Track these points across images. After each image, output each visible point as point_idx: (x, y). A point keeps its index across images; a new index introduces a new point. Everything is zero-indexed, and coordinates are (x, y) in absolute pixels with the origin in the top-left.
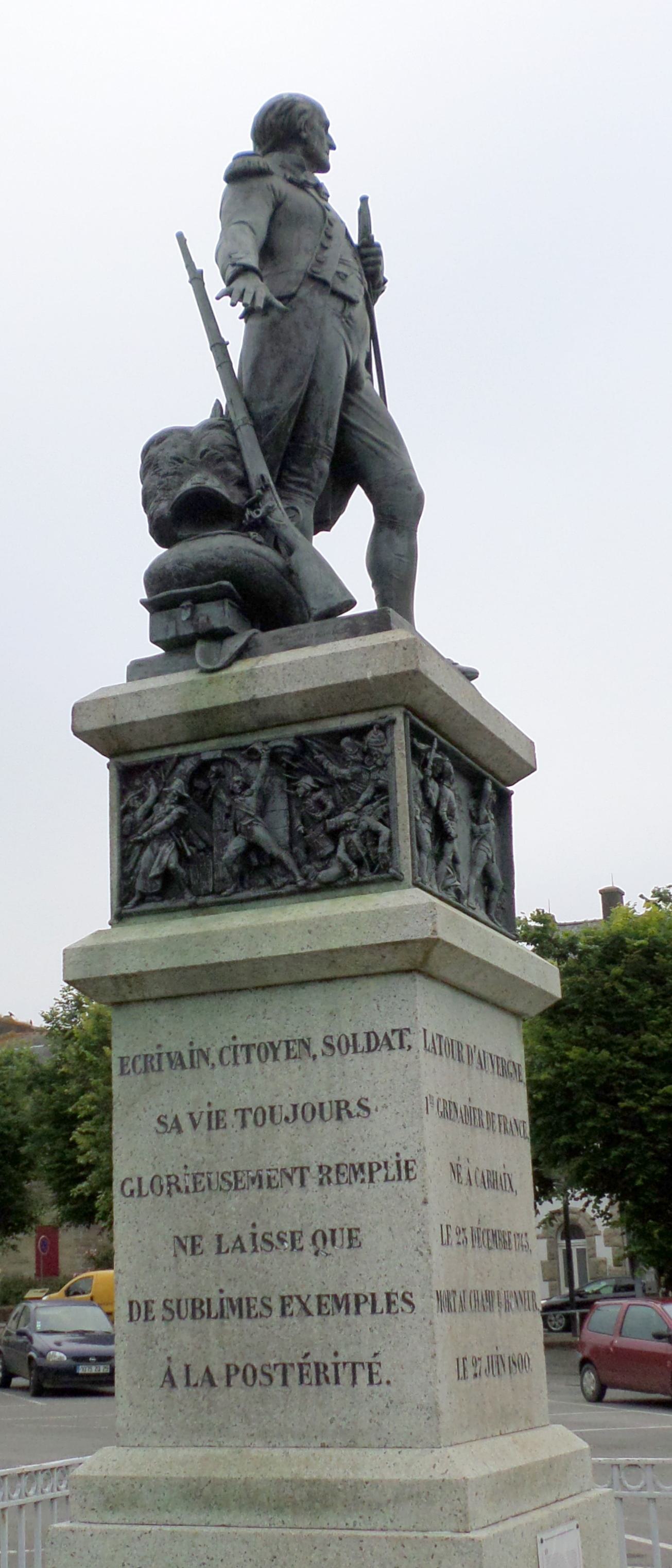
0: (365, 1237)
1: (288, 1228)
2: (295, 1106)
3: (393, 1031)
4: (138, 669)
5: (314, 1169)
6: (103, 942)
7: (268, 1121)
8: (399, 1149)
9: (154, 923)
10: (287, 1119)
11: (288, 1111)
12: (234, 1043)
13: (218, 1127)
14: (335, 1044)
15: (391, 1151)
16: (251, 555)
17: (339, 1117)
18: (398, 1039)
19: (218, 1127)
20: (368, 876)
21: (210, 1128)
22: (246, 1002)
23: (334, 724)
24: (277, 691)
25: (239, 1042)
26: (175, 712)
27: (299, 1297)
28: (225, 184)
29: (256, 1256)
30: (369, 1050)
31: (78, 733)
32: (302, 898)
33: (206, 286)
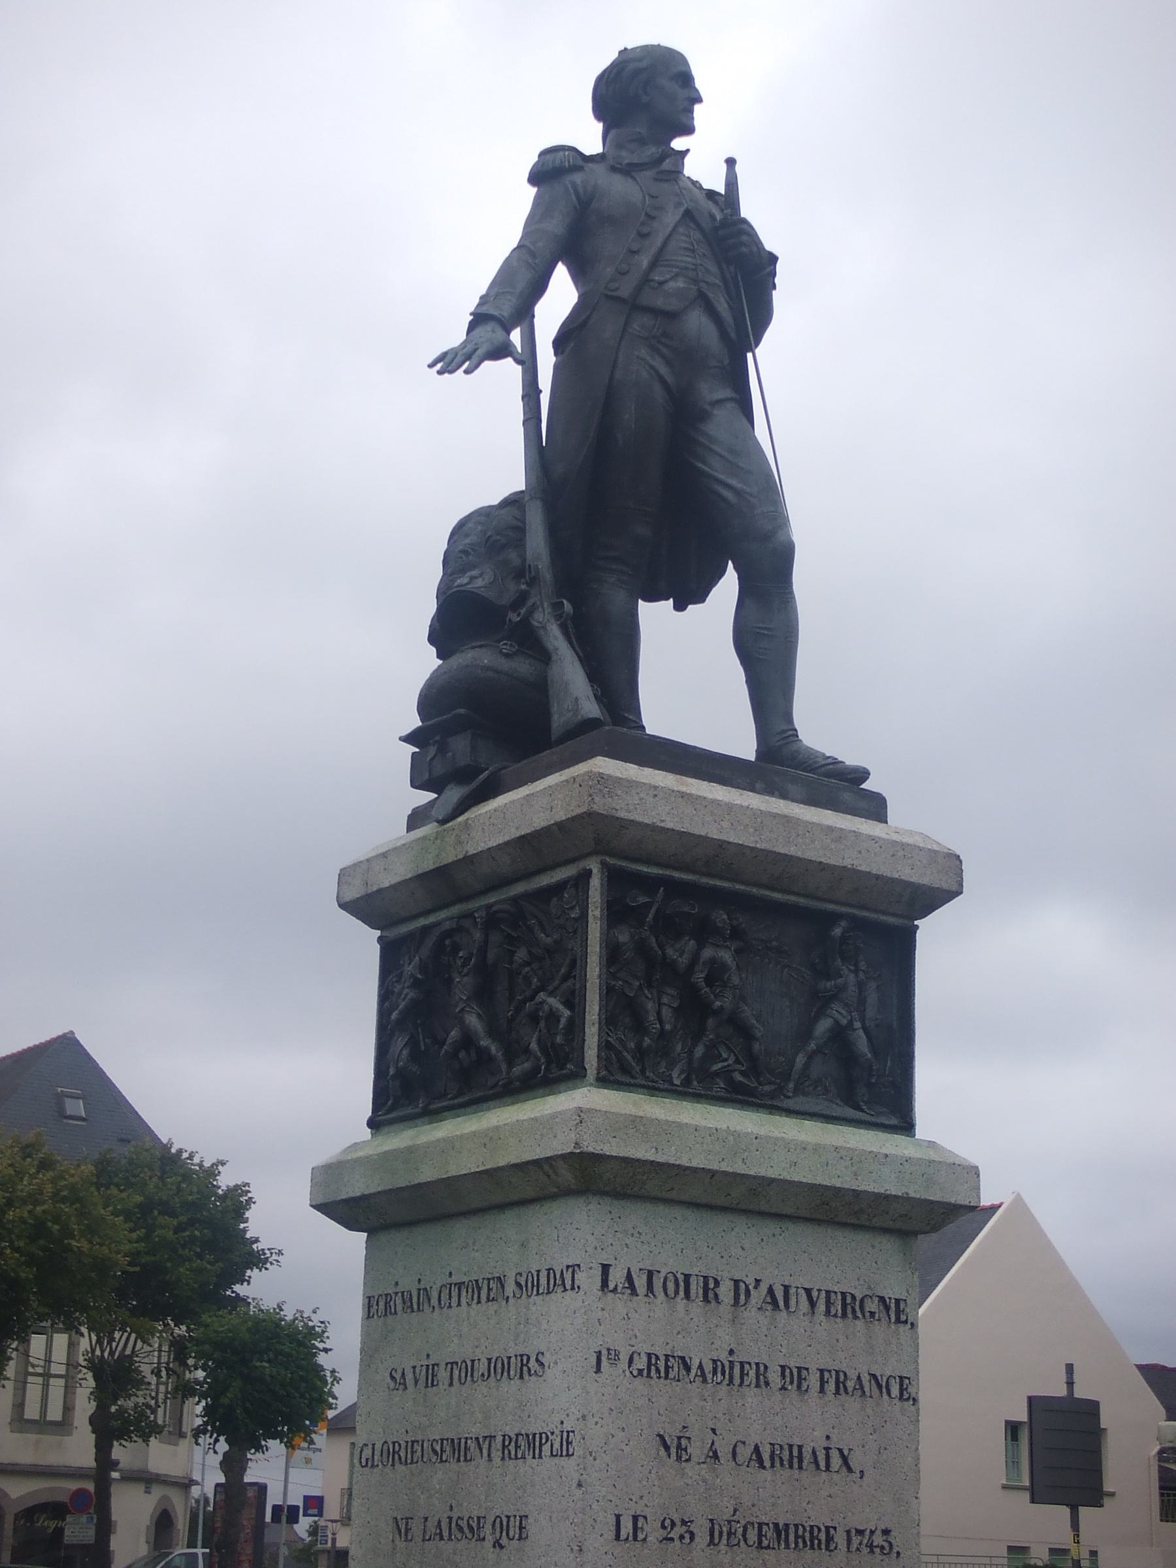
0: (532, 1528)
1: (475, 1514)
2: (489, 1360)
3: (568, 1267)
4: (416, 819)
5: (499, 1439)
6: (410, 1143)
7: (469, 1378)
8: (563, 1417)
9: (424, 1124)
10: (483, 1375)
11: (482, 1367)
12: (449, 1280)
13: (433, 1385)
14: (523, 1283)
15: (556, 1419)
16: (490, 674)
17: (521, 1377)
18: (559, 1281)
19: (433, 1385)
20: (555, 1073)
21: (427, 1386)
22: (461, 1229)
23: (545, 880)
24: (482, 845)
25: (454, 1279)
26: (410, 876)
27: (840, 1450)
28: (533, 191)
29: (451, 1545)
30: (549, 1293)
31: (343, 906)
32: (508, 1100)
33: (535, 320)
